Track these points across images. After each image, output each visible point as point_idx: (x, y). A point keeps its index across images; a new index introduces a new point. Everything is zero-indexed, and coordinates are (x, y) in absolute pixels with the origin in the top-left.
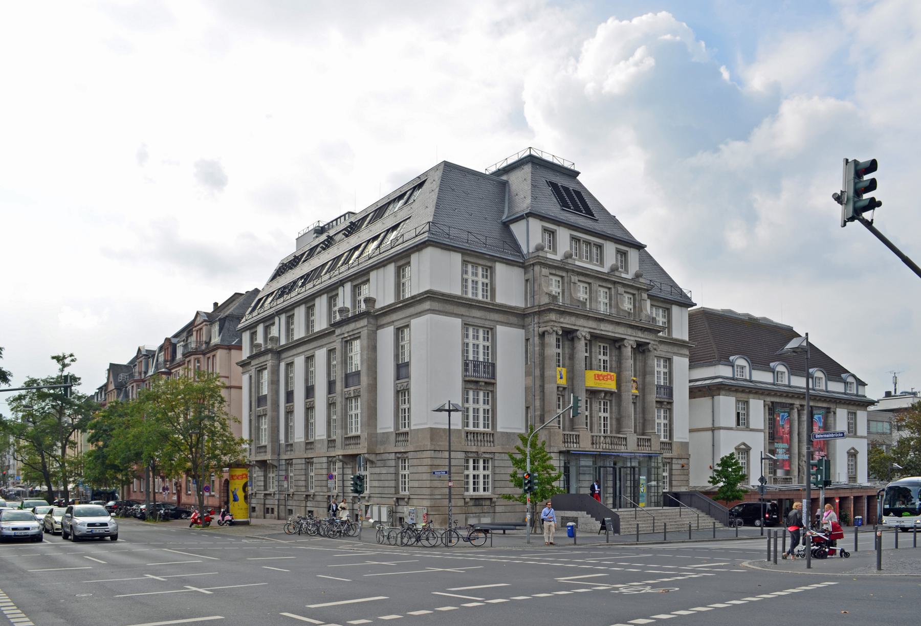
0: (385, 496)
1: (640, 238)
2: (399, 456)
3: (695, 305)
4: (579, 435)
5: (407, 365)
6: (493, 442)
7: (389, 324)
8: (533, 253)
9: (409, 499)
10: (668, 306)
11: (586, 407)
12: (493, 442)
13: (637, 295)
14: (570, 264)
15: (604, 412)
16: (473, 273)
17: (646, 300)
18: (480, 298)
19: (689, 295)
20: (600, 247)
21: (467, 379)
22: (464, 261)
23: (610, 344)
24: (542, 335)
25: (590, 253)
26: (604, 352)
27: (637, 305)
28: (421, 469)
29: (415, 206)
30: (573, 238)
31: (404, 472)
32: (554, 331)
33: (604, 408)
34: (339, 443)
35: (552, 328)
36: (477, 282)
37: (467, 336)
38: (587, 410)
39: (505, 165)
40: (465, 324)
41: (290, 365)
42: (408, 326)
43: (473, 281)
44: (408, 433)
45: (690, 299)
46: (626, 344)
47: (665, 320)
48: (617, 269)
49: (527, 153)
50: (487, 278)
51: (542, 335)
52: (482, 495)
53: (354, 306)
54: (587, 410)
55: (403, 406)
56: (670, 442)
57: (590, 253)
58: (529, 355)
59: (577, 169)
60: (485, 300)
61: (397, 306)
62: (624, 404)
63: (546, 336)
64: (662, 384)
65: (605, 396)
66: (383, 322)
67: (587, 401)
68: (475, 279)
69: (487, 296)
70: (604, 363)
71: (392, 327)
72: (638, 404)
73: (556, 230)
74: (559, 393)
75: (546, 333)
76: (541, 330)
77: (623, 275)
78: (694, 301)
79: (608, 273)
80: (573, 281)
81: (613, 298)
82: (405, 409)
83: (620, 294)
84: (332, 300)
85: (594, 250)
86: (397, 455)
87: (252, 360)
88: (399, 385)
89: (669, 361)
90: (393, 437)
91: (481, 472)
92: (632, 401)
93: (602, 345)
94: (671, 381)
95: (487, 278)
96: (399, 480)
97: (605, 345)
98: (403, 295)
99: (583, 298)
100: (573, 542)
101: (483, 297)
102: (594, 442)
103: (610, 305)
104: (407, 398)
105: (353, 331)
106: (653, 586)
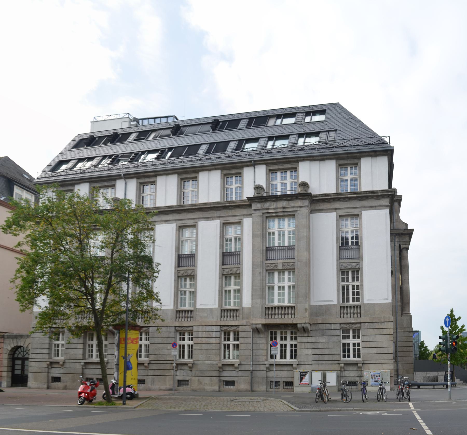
0: (324, 362)
2: (177, 328)
5: (192, 257)
7: (219, 217)
9: (64, 362)
29: (69, 153)
52: (353, 361)
61: (349, 196)
66: (317, 208)
86: (342, 326)
87: (253, 202)
91: (288, 342)
100: (248, 387)
105: (284, 208)
106: (388, 413)
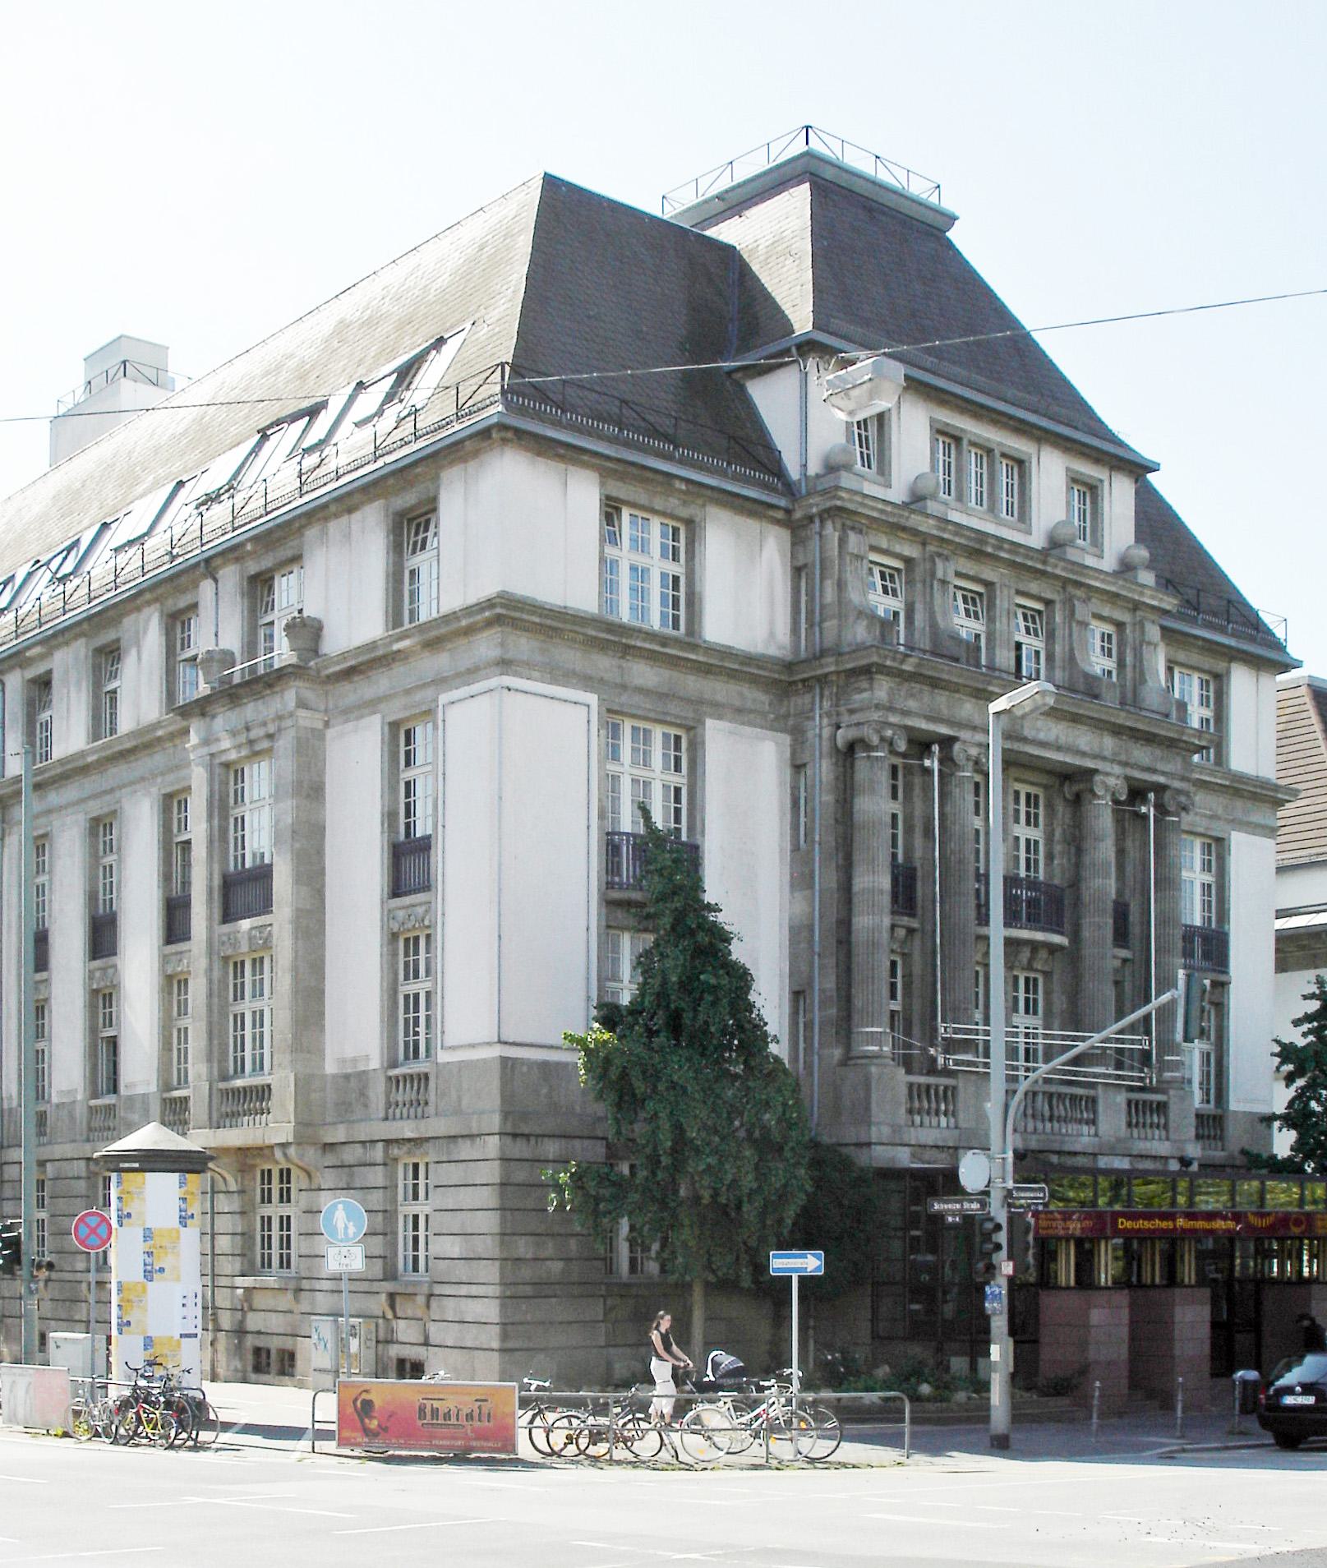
3: (1297, 665)
4: (954, 1088)
5: (424, 846)
6: (954, 1115)
8: (818, 476)
10: (1220, 666)
11: (893, 986)
12: (954, 1115)
13: (1058, 606)
14: (1091, 568)
15: (1027, 1012)
16: (634, 540)
17: (1156, 646)
18: (655, 622)
19: (1279, 633)
20: (1020, 464)
21: (616, 895)
23: (1046, 787)
24: (848, 754)
25: (959, 470)
27: (1129, 660)
28: (467, 1198)
30: (940, 432)
32: (882, 739)
33: (1027, 1000)
35: (878, 732)
37: (615, 757)
38: (893, 996)
39: (724, 183)
41: (41, 844)
42: (429, 714)
44: (426, 1077)
45: (1279, 647)
47: (1208, 713)
49: (798, 148)
50: (675, 558)
51: (848, 754)
53: (251, 649)
54: (893, 996)
55: (411, 988)
56: (1219, 1111)
57: (959, 470)
60: (670, 631)
62: (1090, 985)
67: (893, 964)
68: (641, 560)
69: (676, 619)
70: (1028, 851)
71: (376, 720)
73: (1101, 481)
75: (857, 748)
76: (842, 736)
77: (1090, 561)
79: (905, 505)
80: (940, 574)
81: (1059, 633)
82: (417, 996)
84: (178, 622)
85: (1002, 467)
88: (401, 914)
89: (1217, 849)
90: (377, 1092)
92: (1111, 978)
94: (1223, 915)
95: (675, 558)
96: (395, 1233)
97: (1032, 790)
99: (886, 611)
101: (663, 623)
103: (1050, 658)
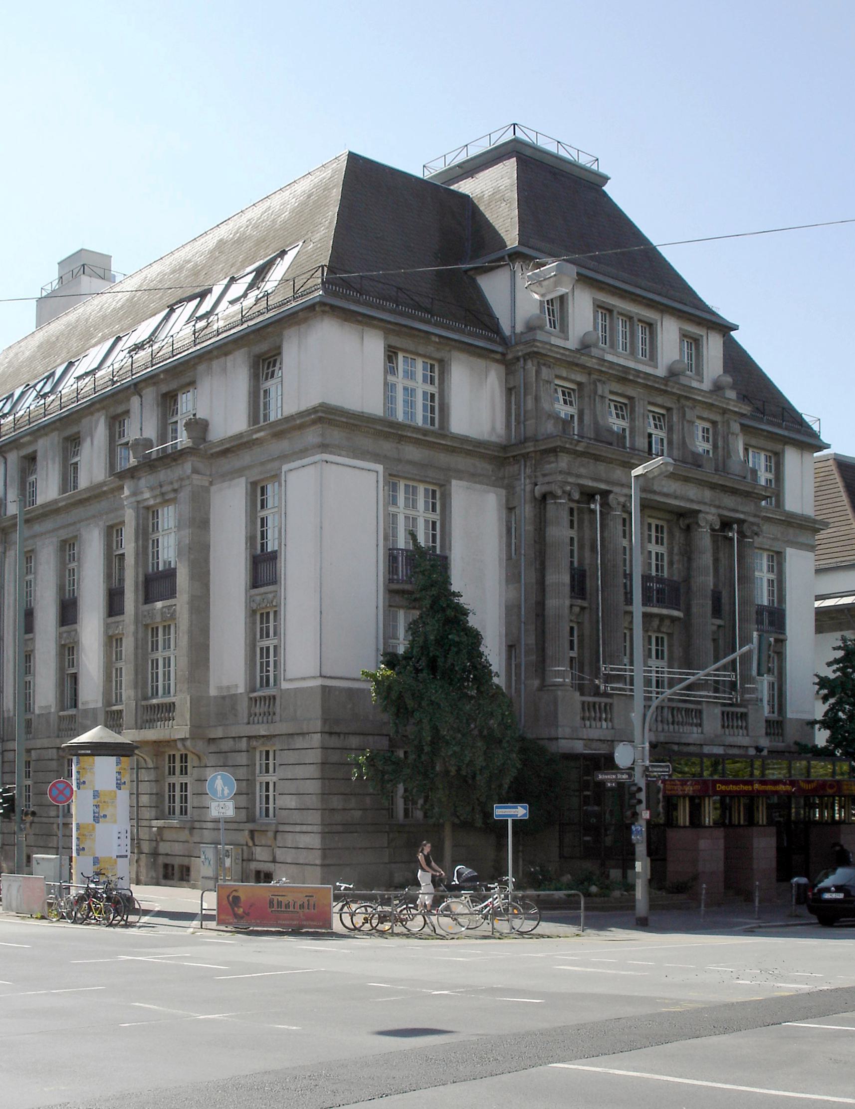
1: (727, 313)
3: (827, 446)
4: (611, 704)
5: (273, 557)
6: (611, 720)
8: (522, 333)
10: (778, 447)
11: (572, 642)
15: (657, 657)
17: (737, 435)
19: (815, 427)
22: (389, 346)
23: (668, 521)
25: (612, 329)
26: (657, 537)
27: (720, 444)
28: (300, 772)
30: (599, 306)
31: (265, 778)
33: (657, 650)
34: (128, 718)
36: (413, 391)
37: (394, 503)
38: (572, 648)
39: (462, 157)
40: (390, 475)
43: (405, 389)
45: (815, 435)
46: (702, 523)
47: (770, 476)
48: (682, 373)
49: (509, 136)
50: (432, 383)
53: (163, 439)
55: (265, 643)
56: (781, 718)
57: (612, 329)
58: (513, 541)
59: (603, 170)
63: (550, 501)
64: (766, 603)
65: (659, 626)
67: (572, 629)
68: (410, 384)
70: (657, 560)
72: (675, 637)
74: (573, 618)
77: (695, 384)
78: (824, 438)
79: (577, 351)
80: (600, 392)
81: (675, 428)
83: (688, 421)
84: (116, 422)
88: (258, 598)
93: (654, 522)
94: (782, 599)
95: (432, 383)
96: (254, 794)
97: (660, 523)
98: (265, 415)
99: (566, 414)
102: (272, 700)
104: (271, 625)
